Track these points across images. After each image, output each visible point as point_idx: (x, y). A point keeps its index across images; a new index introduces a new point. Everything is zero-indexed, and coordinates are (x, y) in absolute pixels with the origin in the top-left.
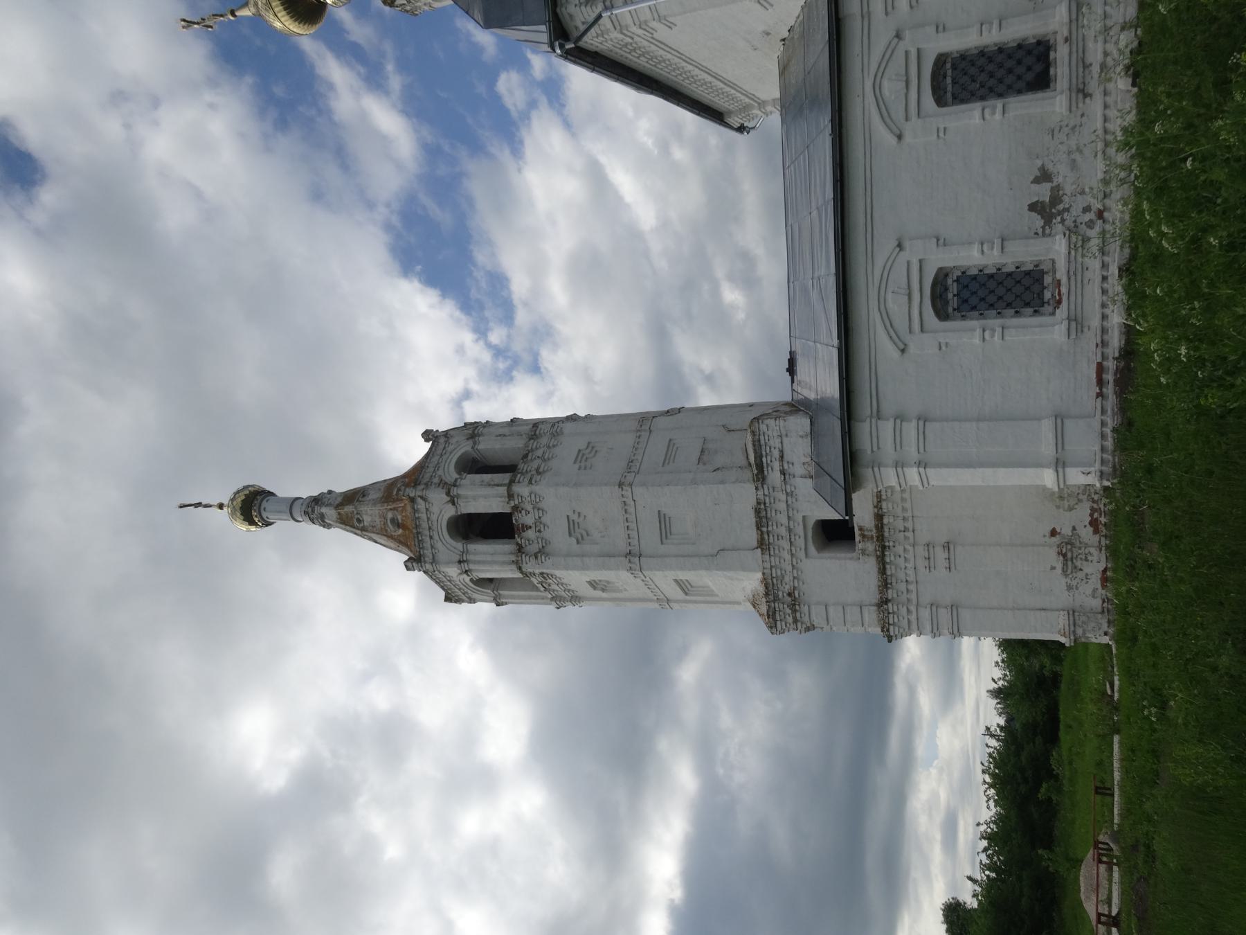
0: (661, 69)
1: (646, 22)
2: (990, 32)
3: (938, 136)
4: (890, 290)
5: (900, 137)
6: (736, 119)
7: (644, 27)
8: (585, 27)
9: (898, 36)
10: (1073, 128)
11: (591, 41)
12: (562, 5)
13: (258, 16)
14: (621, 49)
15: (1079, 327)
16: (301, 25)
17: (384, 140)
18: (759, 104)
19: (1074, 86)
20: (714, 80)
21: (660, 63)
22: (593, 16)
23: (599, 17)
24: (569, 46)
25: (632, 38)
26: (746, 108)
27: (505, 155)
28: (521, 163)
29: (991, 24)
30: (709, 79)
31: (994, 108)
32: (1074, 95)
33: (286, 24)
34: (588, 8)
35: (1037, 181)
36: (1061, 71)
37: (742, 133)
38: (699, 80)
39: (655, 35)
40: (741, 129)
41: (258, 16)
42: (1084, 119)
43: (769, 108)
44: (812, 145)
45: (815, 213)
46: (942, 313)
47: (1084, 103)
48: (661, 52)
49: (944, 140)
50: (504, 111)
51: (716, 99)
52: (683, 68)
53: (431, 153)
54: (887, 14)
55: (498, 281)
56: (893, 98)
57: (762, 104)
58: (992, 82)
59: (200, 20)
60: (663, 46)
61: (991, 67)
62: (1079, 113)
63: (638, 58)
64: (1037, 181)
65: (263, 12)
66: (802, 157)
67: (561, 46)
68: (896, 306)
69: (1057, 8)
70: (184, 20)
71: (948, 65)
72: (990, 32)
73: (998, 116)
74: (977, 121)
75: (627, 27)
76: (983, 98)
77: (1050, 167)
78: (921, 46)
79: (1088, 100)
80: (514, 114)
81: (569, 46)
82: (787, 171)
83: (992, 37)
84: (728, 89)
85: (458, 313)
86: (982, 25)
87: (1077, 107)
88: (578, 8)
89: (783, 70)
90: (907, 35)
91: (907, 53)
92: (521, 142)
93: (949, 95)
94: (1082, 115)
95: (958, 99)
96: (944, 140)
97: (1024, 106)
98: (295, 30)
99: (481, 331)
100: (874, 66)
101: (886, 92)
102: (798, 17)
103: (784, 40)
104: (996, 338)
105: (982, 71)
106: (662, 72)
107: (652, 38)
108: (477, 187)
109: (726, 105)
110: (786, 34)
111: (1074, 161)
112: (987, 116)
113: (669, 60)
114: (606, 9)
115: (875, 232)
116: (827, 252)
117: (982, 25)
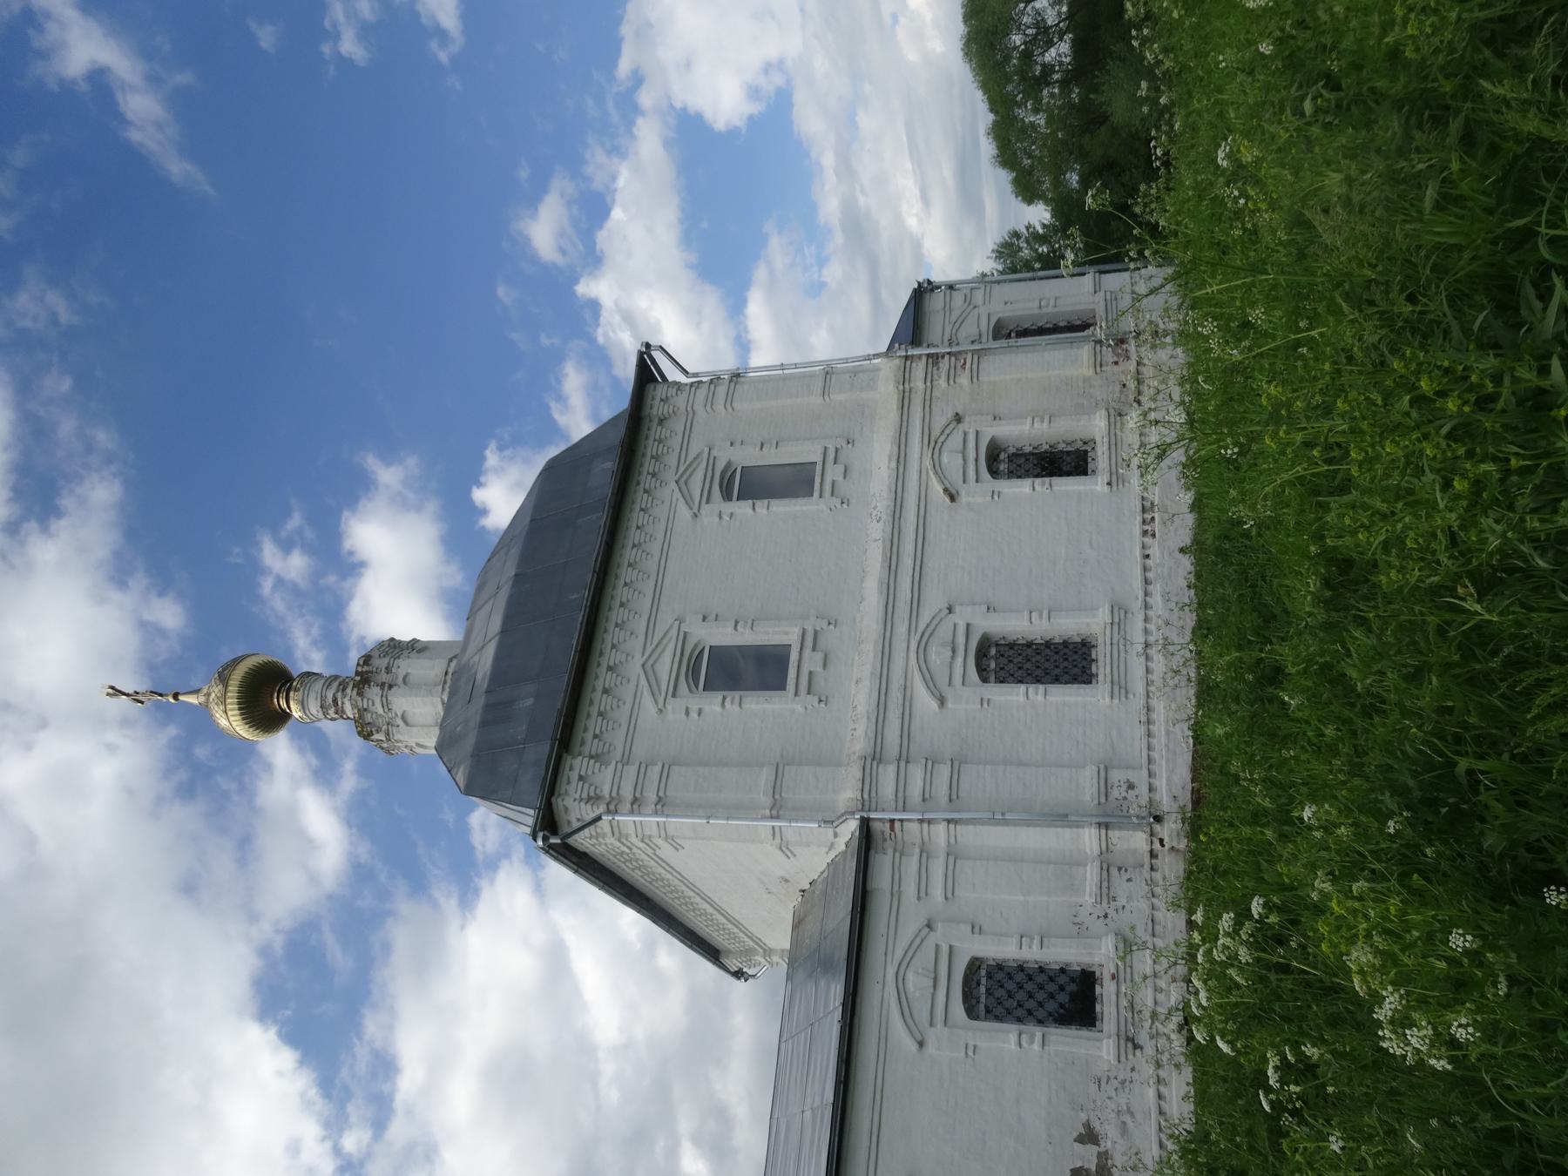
0: (657, 888)
1: (650, 837)
2: (1030, 947)
3: (966, 1053)
4: (912, 967)
5: (921, 1044)
6: (735, 961)
7: (647, 841)
8: (579, 824)
9: (958, 419)
10: (1123, 1082)
11: (582, 841)
12: (560, 795)
13: (205, 706)
14: (615, 856)
15: (1123, 691)
16: (247, 726)
17: (308, 844)
18: (765, 950)
19: (1122, 1033)
20: (715, 912)
21: (657, 880)
22: (592, 816)
23: (599, 818)
24: (554, 840)
25: (630, 849)
26: (749, 952)
27: (450, 905)
28: (467, 914)
29: (1032, 939)
30: (710, 910)
31: (1032, 1037)
32: (1122, 1042)
33: (234, 724)
34: (589, 806)
35: (1081, 1140)
36: (1102, 669)
37: (739, 978)
38: (699, 910)
39: (658, 852)
40: (738, 974)
41: (205, 706)
42: (1135, 1075)
43: (776, 959)
44: (816, 1025)
45: (808, 1114)
46: (994, 473)
47: (1134, 1055)
48: (660, 870)
49: (973, 1059)
50: (469, 849)
51: (715, 934)
52: (683, 892)
53: (359, 874)
54: (919, 898)
55: (385, 1065)
56: (917, 995)
57: (768, 952)
58: (1030, 1004)
59: (131, 692)
60: (664, 864)
61: (1030, 986)
62: (1129, 1066)
63: (633, 870)
64: (1081, 1140)
65: (213, 707)
66: (803, 1034)
67: (545, 839)
68: (916, 983)
69: (1104, 940)
70: (112, 688)
71: (983, 973)
72: (1030, 947)
73: (1036, 1047)
74: (1013, 1047)
75: (627, 837)
76: (1020, 1020)
77: (1096, 1125)
78: (953, 944)
79: (1138, 1052)
80: (479, 856)
81: (554, 840)
82: (783, 1045)
83: (1032, 954)
84: (730, 926)
85: (313, 1093)
86: (1022, 937)
87: (1126, 1058)
88: (577, 803)
89: (797, 925)
90: (939, 926)
91: (965, 434)
92: (477, 892)
93: (982, 1007)
94: (1133, 1069)
95: (992, 1014)
96: (973, 1059)
97: (1067, 1041)
98: (241, 732)
99: (334, 1126)
100: (899, 953)
101: (910, 987)
102: (822, 873)
103: (803, 891)
104: (1034, 947)
105: (1021, 988)
106: (657, 891)
107: (655, 854)
108: (401, 935)
109: (725, 943)
110: (807, 886)
111: (1124, 1123)
112: (1024, 1044)
113: (668, 880)
114: (608, 812)
115: (880, 1162)
116: (819, 1152)
117: (1022, 937)
